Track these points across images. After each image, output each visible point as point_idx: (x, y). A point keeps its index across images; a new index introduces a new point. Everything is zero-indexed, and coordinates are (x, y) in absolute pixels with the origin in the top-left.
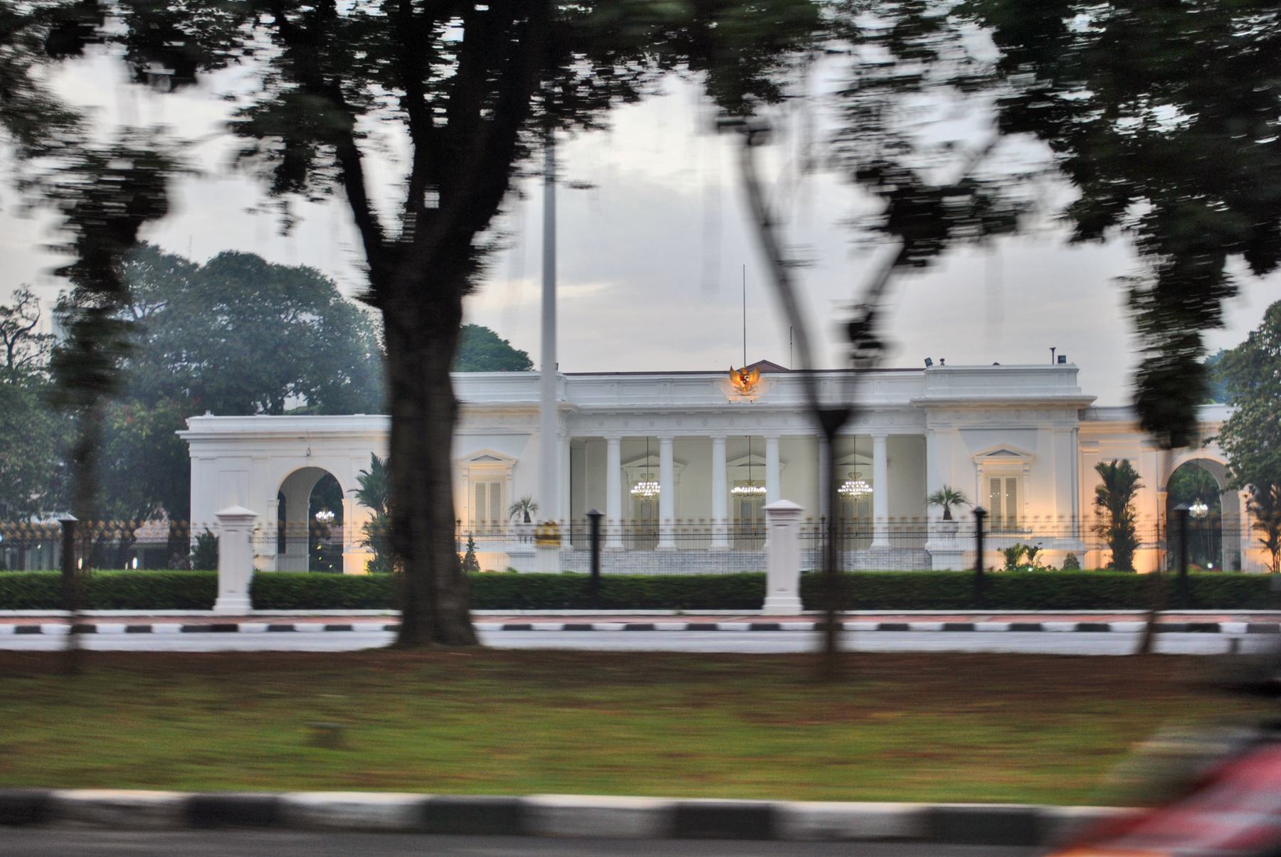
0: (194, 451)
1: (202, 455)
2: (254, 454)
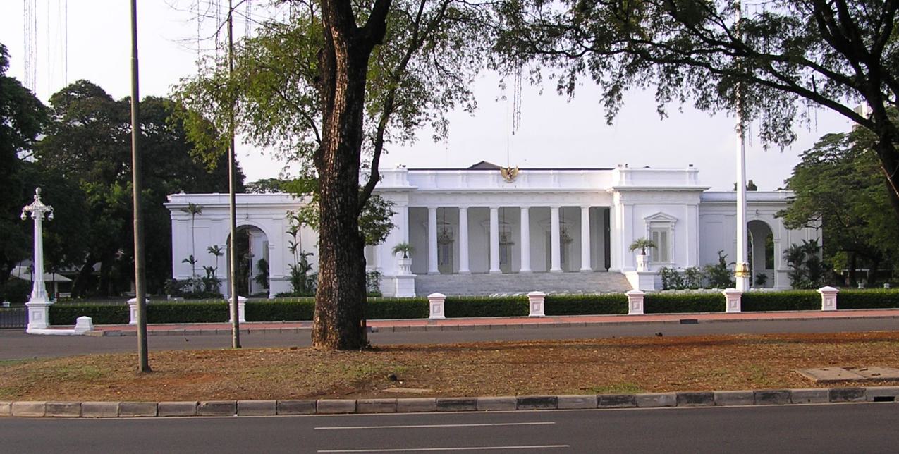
0: (174, 215)
1: (179, 218)
2: (274, 217)
